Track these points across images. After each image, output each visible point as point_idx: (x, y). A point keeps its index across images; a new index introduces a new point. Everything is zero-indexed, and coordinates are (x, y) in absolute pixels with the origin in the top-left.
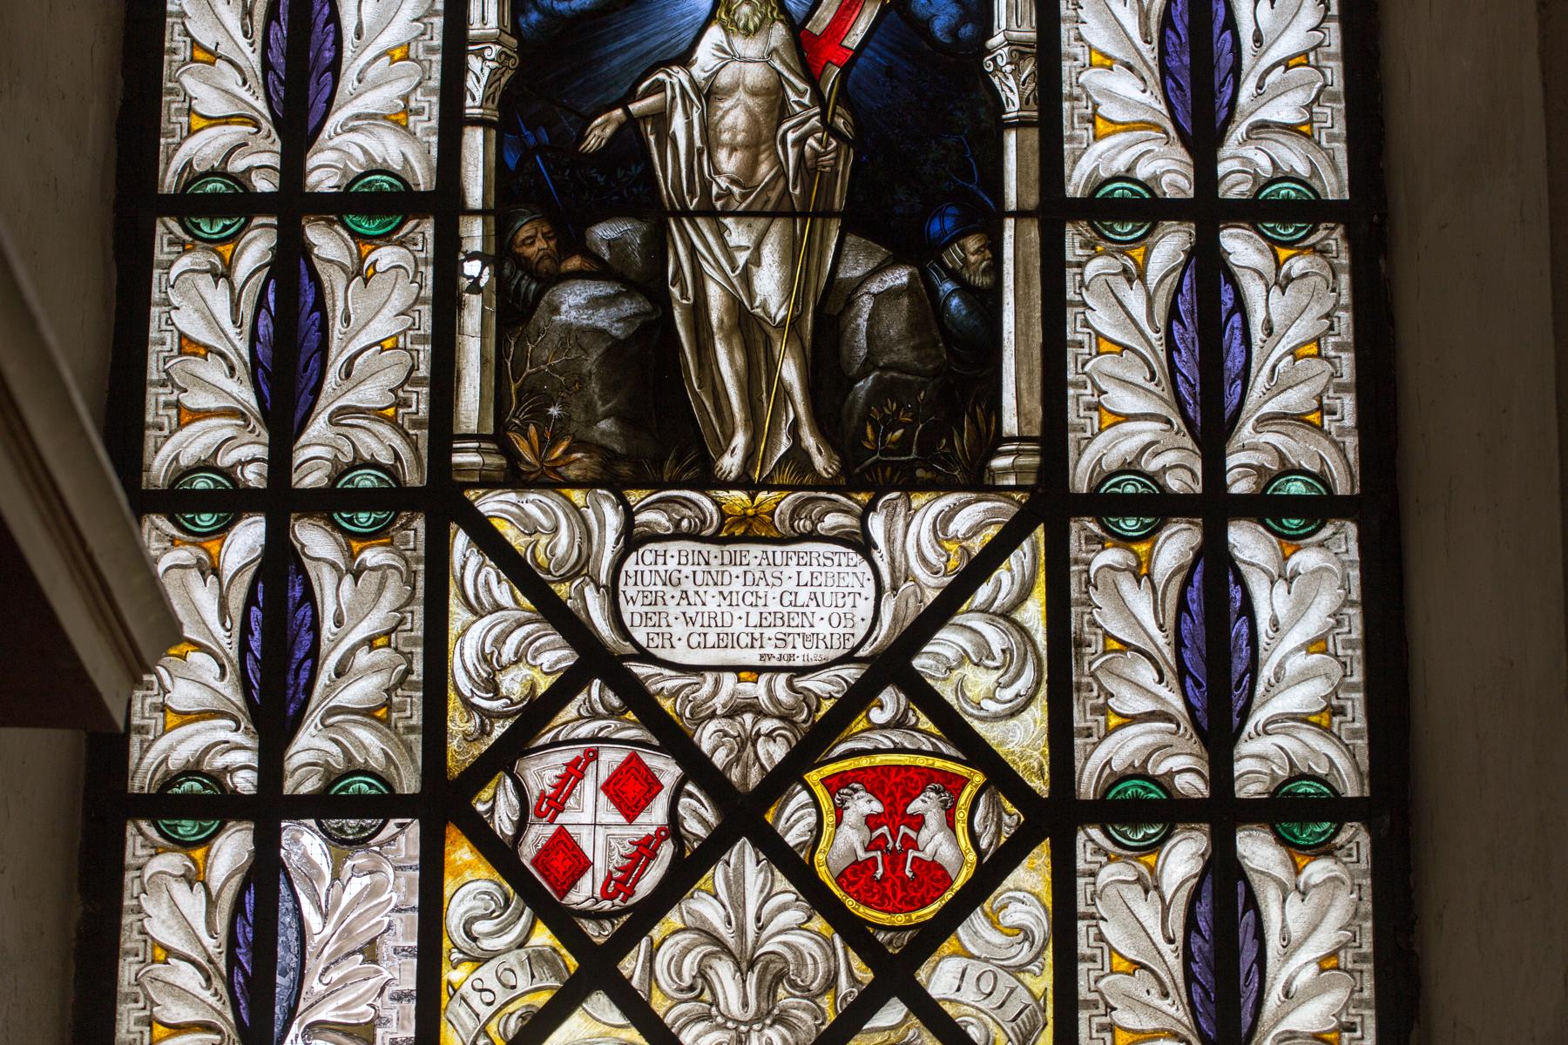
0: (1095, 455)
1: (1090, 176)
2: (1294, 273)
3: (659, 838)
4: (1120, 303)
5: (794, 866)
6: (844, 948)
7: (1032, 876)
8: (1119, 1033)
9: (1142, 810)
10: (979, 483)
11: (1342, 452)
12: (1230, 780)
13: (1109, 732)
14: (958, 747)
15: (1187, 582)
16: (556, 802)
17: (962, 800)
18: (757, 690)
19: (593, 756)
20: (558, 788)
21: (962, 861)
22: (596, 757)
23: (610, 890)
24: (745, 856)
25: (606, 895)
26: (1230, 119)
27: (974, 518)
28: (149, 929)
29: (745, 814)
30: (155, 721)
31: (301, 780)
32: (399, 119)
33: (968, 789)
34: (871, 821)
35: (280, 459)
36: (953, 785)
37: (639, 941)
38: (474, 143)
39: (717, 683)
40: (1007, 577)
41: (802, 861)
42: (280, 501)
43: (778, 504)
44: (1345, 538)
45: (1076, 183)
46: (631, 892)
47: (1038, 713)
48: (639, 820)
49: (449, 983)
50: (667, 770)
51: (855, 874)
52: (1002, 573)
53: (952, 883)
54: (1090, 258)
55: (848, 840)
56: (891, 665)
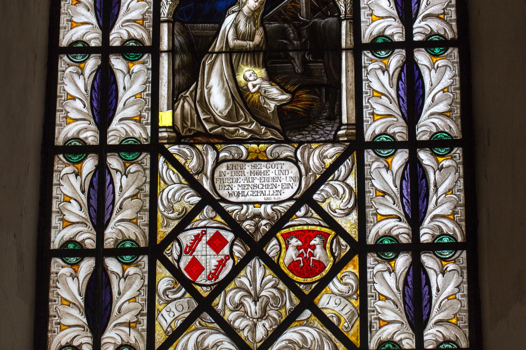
0: (372, 129)
1: (372, 134)
2: (439, 66)
3: (227, 258)
4: (381, 77)
5: (273, 265)
6: (289, 291)
7: (352, 268)
8: (375, 116)
9: (388, 248)
10: (335, 141)
11: (451, 26)
12: (415, 136)
13: (378, 222)
14: (328, 224)
15: (94, 176)
16: (192, 249)
17: (328, 240)
18: (261, 210)
19: (204, 233)
20: (192, 244)
21: (329, 261)
22: (206, 233)
23: (210, 277)
24: (256, 262)
25: (209, 279)
26: (425, 216)
27: (332, 151)
28: (66, 89)
29: (256, 248)
30: (56, 328)
31: (109, 244)
32: (138, 119)
33: (331, 236)
34: (298, 248)
35: (100, 238)
36: (325, 236)
37: (221, 293)
38: (165, 28)
39: (248, 209)
40: (343, 169)
41: (274, 262)
42: (102, 150)
43: (267, 148)
44: (454, 52)
45: (366, 39)
46: (217, 277)
47: (354, 216)
48: (220, 253)
49: (158, 309)
50: (229, 236)
51: (293, 266)
52: (342, 168)
53: (325, 267)
54: (376, 265)
55: (291, 254)
56: (305, 198)
